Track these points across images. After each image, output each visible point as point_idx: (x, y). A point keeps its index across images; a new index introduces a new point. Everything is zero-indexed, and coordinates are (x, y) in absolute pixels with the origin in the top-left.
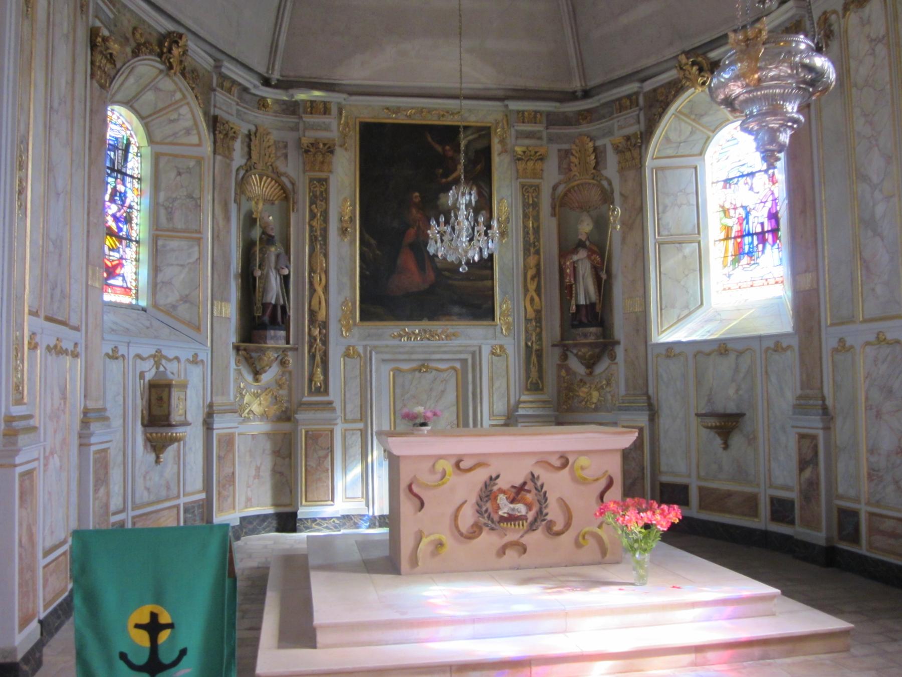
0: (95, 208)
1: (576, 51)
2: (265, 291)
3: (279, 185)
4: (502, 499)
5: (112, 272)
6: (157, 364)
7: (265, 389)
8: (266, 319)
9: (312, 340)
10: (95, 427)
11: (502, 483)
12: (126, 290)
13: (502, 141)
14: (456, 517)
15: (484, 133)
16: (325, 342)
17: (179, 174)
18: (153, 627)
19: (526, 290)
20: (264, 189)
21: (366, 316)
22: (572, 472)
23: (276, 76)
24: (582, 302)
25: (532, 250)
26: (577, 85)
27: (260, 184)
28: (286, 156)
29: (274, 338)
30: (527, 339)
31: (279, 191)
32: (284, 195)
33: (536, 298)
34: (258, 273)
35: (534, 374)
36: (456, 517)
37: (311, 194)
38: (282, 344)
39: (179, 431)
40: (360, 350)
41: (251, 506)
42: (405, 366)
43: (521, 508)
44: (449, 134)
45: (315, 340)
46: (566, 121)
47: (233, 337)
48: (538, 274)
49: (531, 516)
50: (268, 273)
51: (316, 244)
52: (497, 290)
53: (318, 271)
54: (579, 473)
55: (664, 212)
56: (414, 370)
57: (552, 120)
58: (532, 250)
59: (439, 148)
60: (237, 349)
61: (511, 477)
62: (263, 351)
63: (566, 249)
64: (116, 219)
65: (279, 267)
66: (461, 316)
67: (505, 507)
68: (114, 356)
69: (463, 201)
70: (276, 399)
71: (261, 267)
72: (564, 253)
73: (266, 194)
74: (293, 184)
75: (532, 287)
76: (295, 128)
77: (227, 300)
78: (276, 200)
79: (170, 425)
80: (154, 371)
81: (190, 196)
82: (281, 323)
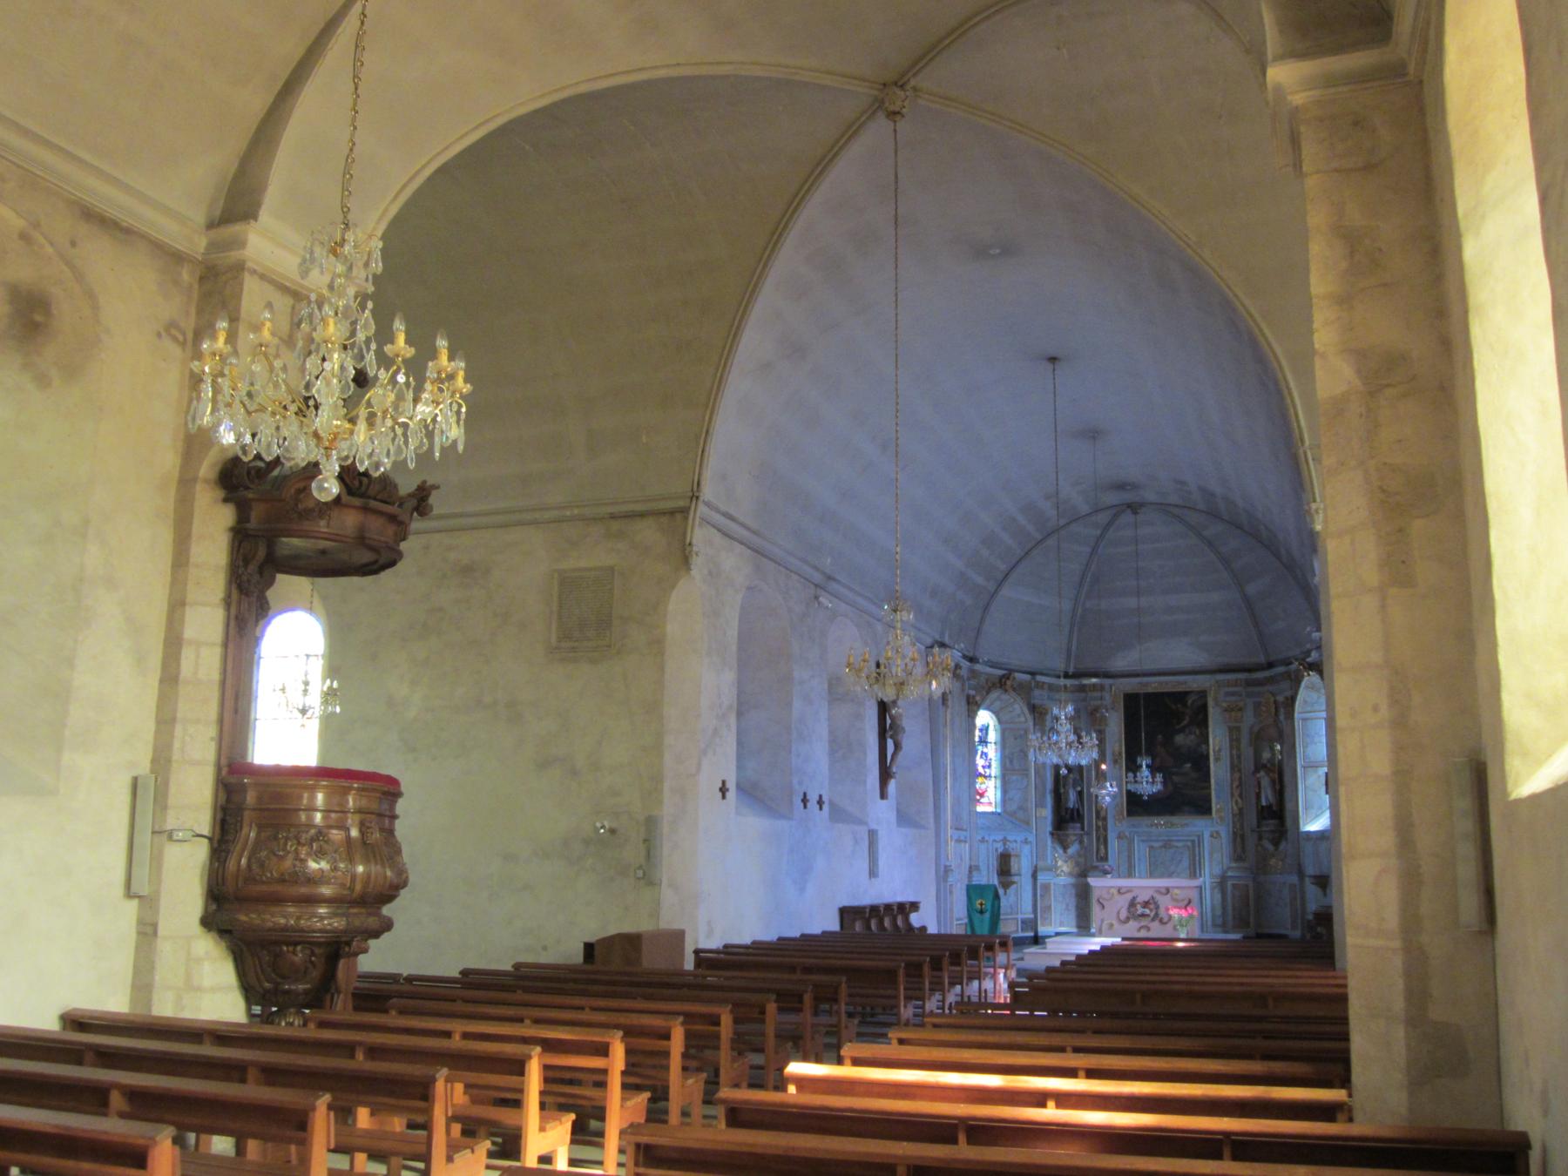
0: (973, 764)
2: (1067, 800)
4: (1139, 907)
5: (982, 795)
6: (1005, 844)
7: (1071, 857)
8: (1068, 816)
9: (1098, 828)
10: (975, 873)
11: (1139, 900)
12: (990, 804)
13: (1215, 699)
14: (1118, 913)
15: (1203, 694)
16: (1105, 829)
17: (1016, 739)
18: (981, 904)
19: (1232, 795)
21: (1130, 813)
22: (1171, 896)
23: (1071, 671)
24: (1264, 804)
25: (1236, 769)
26: (1262, 659)
29: (1074, 828)
30: (1234, 827)
33: (1239, 800)
34: (1062, 790)
35: (1239, 850)
36: (1118, 913)
38: (1078, 832)
39: (1015, 879)
40: (1127, 834)
41: (1063, 926)
42: (1156, 845)
43: (1147, 911)
44: (1181, 697)
46: (1260, 683)
47: (1049, 828)
48: (1240, 785)
49: (1152, 914)
52: (1213, 793)
54: (1175, 897)
55: (1307, 747)
56: (1161, 847)
57: (1249, 683)
58: (1236, 769)
59: (1174, 707)
60: (1052, 834)
61: (1144, 897)
62: (1067, 836)
63: (1259, 766)
64: (984, 767)
66: (1190, 813)
67: (1140, 910)
68: (983, 840)
69: (1144, 763)
70: (1077, 864)
71: (1064, 787)
72: (1257, 770)
75: (1236, 793)
76: (1084, 700)
77: (1045, 807)
79: (1011, 875)
80: (1002, 848)
81: (1021, 751)
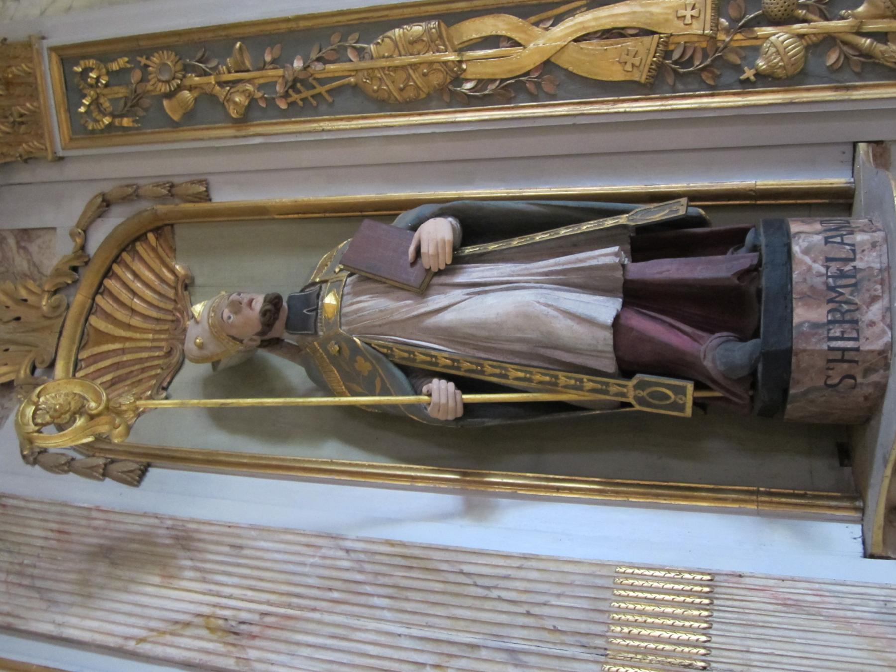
1: (753, 621)
3: (117, 259)
20: (136, 321)
27: (115, 339)
28: (25, 235)
31: (142, 259)
32: (151, 236)
37: (126, 122)
45: (830, 40)
50: (449, 335)
51: (322, 82)
53: (452, 57)
65: (414, 276)
73: (154, 313)
74: (105, 204)
78: (173, 271)
82: (741, 260)
